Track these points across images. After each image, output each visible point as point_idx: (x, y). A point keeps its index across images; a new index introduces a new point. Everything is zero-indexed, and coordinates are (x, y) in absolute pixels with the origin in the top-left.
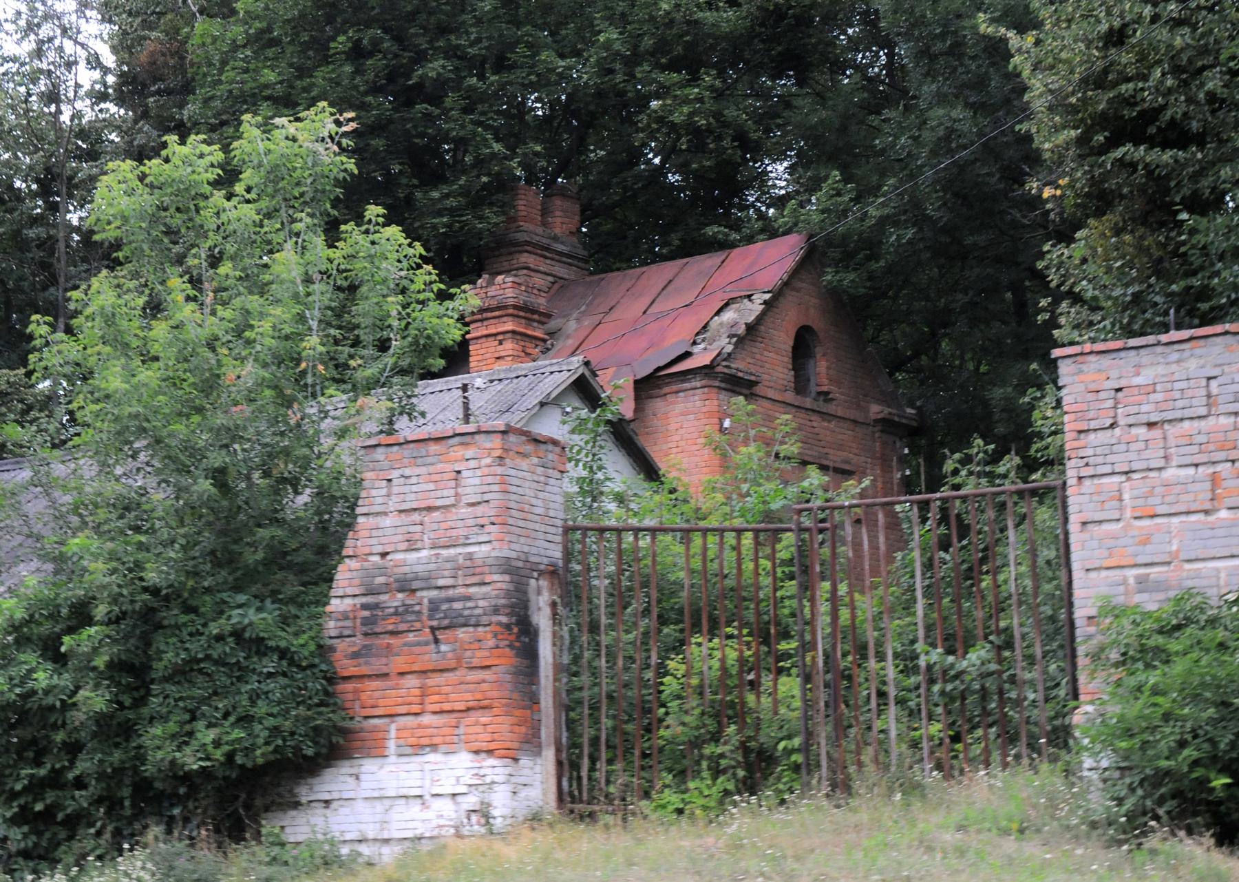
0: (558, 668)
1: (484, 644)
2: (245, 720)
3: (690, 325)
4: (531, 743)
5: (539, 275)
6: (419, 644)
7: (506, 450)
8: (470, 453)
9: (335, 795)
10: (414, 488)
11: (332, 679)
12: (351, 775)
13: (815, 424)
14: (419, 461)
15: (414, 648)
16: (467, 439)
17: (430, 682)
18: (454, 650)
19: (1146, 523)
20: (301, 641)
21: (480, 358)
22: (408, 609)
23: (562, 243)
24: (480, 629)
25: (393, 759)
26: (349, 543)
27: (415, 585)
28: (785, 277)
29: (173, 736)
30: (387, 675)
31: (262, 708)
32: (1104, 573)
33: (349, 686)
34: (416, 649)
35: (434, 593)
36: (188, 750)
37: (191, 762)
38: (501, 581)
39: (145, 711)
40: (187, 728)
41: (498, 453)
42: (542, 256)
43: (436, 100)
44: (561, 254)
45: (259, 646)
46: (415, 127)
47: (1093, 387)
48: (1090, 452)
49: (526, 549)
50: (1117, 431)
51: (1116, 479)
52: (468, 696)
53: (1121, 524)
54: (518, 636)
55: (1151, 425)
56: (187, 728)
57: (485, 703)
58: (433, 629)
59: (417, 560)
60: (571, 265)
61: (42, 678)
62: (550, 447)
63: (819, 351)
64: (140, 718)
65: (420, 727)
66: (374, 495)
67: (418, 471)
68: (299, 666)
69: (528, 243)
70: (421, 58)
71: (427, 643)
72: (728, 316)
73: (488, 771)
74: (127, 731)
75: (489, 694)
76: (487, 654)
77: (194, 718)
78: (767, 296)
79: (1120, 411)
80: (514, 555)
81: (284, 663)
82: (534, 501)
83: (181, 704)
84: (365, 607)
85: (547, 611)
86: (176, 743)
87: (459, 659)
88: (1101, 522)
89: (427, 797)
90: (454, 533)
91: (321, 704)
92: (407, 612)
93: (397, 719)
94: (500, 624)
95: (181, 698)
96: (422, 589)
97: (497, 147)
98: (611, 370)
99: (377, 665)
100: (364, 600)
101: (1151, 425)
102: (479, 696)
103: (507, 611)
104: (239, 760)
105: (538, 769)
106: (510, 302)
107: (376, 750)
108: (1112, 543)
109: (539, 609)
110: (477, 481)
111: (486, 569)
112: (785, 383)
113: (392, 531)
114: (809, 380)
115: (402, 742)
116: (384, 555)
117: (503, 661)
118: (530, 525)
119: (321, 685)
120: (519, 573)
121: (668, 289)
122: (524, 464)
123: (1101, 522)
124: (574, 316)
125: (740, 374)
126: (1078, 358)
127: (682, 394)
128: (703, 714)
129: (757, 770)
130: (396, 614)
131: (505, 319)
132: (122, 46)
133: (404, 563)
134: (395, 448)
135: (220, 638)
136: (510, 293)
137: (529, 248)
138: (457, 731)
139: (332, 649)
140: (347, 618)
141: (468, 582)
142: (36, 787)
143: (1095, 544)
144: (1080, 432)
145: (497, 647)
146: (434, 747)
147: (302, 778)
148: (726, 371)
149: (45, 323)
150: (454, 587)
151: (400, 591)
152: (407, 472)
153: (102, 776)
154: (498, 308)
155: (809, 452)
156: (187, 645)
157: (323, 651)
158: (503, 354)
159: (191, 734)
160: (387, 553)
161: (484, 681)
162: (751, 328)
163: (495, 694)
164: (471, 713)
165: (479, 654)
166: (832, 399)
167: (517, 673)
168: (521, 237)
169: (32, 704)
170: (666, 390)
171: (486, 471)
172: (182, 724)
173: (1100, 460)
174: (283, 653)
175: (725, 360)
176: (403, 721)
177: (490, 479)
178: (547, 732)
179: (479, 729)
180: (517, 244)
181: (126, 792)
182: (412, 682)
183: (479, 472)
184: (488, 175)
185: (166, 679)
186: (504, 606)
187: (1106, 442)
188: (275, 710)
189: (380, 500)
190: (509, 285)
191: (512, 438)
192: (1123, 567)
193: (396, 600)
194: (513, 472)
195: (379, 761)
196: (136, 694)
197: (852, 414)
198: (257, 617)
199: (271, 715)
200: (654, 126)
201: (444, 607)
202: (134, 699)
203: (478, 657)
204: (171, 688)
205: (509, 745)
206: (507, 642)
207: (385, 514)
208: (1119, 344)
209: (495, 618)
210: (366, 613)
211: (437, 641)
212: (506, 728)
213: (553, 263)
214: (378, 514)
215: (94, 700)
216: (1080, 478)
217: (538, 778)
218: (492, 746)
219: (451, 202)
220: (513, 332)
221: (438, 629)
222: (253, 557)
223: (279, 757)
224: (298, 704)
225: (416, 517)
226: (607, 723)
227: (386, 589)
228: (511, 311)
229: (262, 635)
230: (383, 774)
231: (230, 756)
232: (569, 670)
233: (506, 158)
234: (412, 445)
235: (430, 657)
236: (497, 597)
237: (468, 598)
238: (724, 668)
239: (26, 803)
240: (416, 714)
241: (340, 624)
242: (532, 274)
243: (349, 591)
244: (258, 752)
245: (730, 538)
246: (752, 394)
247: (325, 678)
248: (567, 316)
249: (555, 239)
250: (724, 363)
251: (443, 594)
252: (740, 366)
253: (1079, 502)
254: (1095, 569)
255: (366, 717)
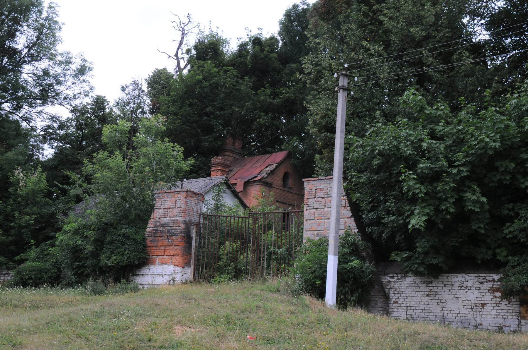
0: (196, 246)
1: (177, 240)
2: (123, 255)
4: (188, 264)
11: (145, 246)
19: (320, 221)
27: (165, 226)
29: (107, 257)
33: (149, 248)
35: (169, 228)
36: (110, 261)
37: (109, 264)
38: (183, 226)
43: (209, 116)
45: (128, 238)
51: (314, 210)
54: (186, 239)
55: (322, 198)
59: (165, 220)
63: (290, 178)
70: (207, 107)
72: (268, 168)
74: (98, 256)
84: (154, 230)
85: (195, 233)
87: (173, 244)
91: (141, 252)
97: (221, 127)
99: (155, 244)
101: (322, 198)
105: (190, 270)
107: (153, 263)
116: (159, 218)
120: (188, 224)
122: (192, 199)
132: (151, 101)
135: (119, 235)
136: (220, 161)
139: (147, 239)
146: (166, 263)
153: (92, 266)
157: (144, 239)
159: (111, 257)
168: (226, 148)
169: (78, 248)
174: (134, 240)
182: (163, 248)
185: (107, 244)
191: (189, 193)
193: (160, 229)
203: (177, 243)
208: (324, 178)
211: (168, 239)
215: (90, 248)
217: (189, 272)
219: (210, 139)
225: (167, 210)
226: (206, 260)
227: (159, 226)
230: (155, 269)
231: (118, 263)
232: (200, 247)
235: (166, 242)
238: (233, 249)
249: (236, 149)
252: (269, 180)
253: (307, 215)
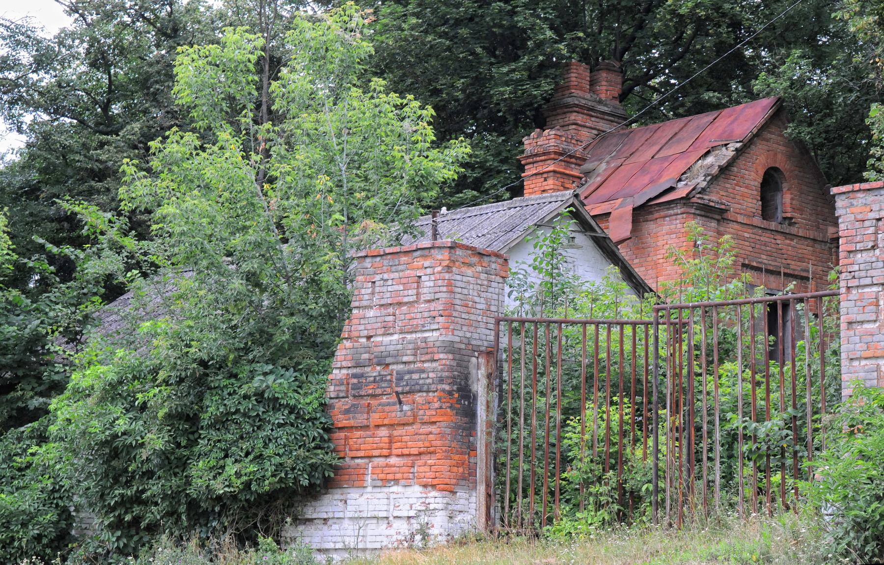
0: (489, 424)
1: (431, 404)
3: (681, 166)
4: (467, 478)
5: (586, 129)
6: (388, 404)
7: (454, 262)
8: (427, 263)
9: (330, 515)
10: (390, 289)
12: (341, 501)
13: (778, 242)
14: (394, 268)
15: (386, 408)
16: (426, 252)
17: (395, 433)
18: (412, 410)
20: (308, 400)
21: (531, 191)
22: (382, 378)
23: (606, 105)
24: (431, 394)
25: (369, 489)
26: (346, 328)
28: (755, 131)
30: (368, 426)
31: (272, 448)
32: (863, 363)
33: (342, 435)
34: (387, 408)
37: (219, 488)
39: (196, 449)
40: (221, 462)
41: (446, 263)
42: (588, 115)
44: (603, 113)
45: (275, 404)
46: (493, 20)
47: (860, 217)
48: (856, 268)
49: (468, 335)
50: (877, 252)
51: (875, 289)
52: (420, 444)
53: (877, 324)
56: (221, 462)
57: (432, 449)
58: (397, 394)
59: (390, 342)
60: (612, 121)
61: (122, 425)
62: (494, 259)
63: (785, 186)
64: (192, 455)
65: (387, 466)
66: (362, 292)
67: (392, 276)
68: (303, 419)
69: (577, 106)
71: (394, 404)
72: (710, 160)
73: (432, 500)
75: (434, 443)
76: (434, 413)
77: (226, 456)
78: (738, 145)
79: (880, 236)
80: (457, 339)
81: (293, 416)
82: (477, 299)
83: (218, 445)
84: (355, 376)
85: (484, 381)
86: (212, 474)
87: (415, 416)
88: (862, 322)
89: (391, 518)
90: (415, 322)
91: (318, 447)
92: (382, 380)
93: (373, 459)
94: (444, 390)
95: (219, 441)
96: (393, 363)
98: (620, 200)
99: (360, 419)
100: (355, 371)
102: (427, 444)
103: (449, 381)
104: (254, 487)
106: (552, 149)
108: (869, 339)
109: (478, 380)
110: (432, 284)
111: (436, 350)
112: (754, 211)
113: (374, 320)
114: (777, 208)
115: (375, 477)
116: (369, 338)
117: (445, 418)
118: (473, 317)
119: (319, 433)
120: (461, 355)
121: (674, 139)
122: (469, 272)
123: (862, 322)
124: (606, 160)
125: (712, 204)
126: (851, 195)
127: (667, 219)
128: (592, 461)
129: (627, 505)
130: (374, 381)
131: (549, 162)
133: (380, 344)
134: (378, 259)
135: (246, 397)
136: (552, 142)
137: (577, 109)
138: (412, 470)
139: (332, 406)
140: (342, 384)
141: (423, 359)
142: (126, 503)
143: (857, 339)
144: (850, 252)
145: (441, 408)
146: (396, 481)
147: (308, 501)
148: (699, 201)
149: (133, 165)
150: (414, 362)
151: (378, 365)
152: (386, 276)
154: (544, 154)
155: (773, 263)
156: (226, 402)
158: (547, 188)
159: (223, 467)
160: (371, 337)
161: (431, 433)
162: (724, 170)
163: (439, 443)
164: (422, 457)
165: (428, 413)
166: (795, 223)
167: (457, 427)
168: (570, 100)
169: (118, 443)
170: (656, 215)
171: (438, 276)
172: (218, 460)
173: (863, 274)
174: (292, 409)
175: (699, 193)
176: (377, 461)
177: (440, 283)
178: (480, 472)
179: (427, 469)
180: (568, 106)
181: (182, 509)
182: (383, 432)
183: (433, 278)
184: (544, 55)
185: (210, 426)
186: (447, 377)
187: (868, 259)
188: (281, 451)
189: (366, 297)
190: (552, 136)
191: (459, 252)
192: (878, 357)
194: (459, 277)
195: (361, 491)
196: (191, 437)
197: (811, 234)
198: (278, 383)
199: (278, 455)
200: (668, 17)
201: (407, 377)
202: (189, 439)
204: (214, 435)
205: (447, 481)
206: (449, 405)
207: (371, 308)
209: (440, 387)
210: (355, 381)
211: (400, 402)
212: (447, 468)
213: (598, 120)
214: (365, 307)
215: (156, 441)
216: (848, 288)
217: (471, 506)
218: (435, 482)
219: (517, 76)
220: (554, 172)
221: (403, 393)
222: (282, 337)
223: (283, 486)
224: (300, 447)
225: (391, 310)
227: (370, 363)
228: (553, 156)
229: (276, 395)
230: (362, 500)
231: (247, 485)
233: (556, 42)
234: (389, 257)
235: (396, 414)
236: (442, 370)
237: (423, 371)
239: (119, 515)
240: (386, 456)
241: (337, 388)
242: (580, 128)
243: (344, 364)
244: (267, 482)
245: (591, 328)
246: (723, 219)
247: (324, 429)
248: (601, 160)
249: (600, 102)
250: (698, 196)
251: (407, 368)
252: (713, 198)
253: (848, 308)
254: (857, 359)
255: (353, 458)
